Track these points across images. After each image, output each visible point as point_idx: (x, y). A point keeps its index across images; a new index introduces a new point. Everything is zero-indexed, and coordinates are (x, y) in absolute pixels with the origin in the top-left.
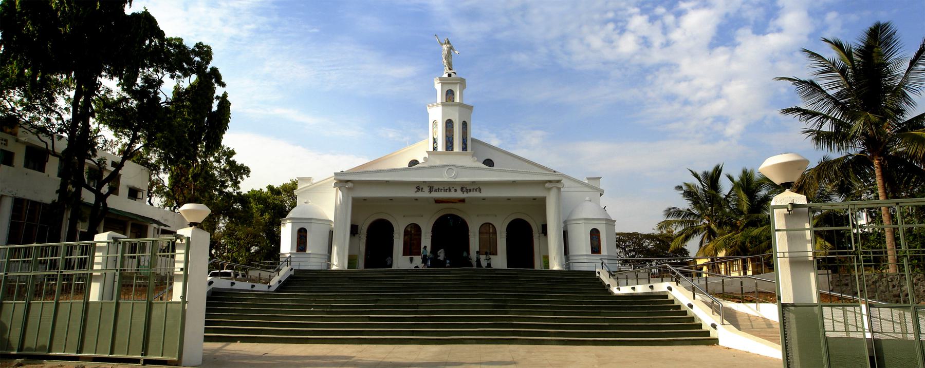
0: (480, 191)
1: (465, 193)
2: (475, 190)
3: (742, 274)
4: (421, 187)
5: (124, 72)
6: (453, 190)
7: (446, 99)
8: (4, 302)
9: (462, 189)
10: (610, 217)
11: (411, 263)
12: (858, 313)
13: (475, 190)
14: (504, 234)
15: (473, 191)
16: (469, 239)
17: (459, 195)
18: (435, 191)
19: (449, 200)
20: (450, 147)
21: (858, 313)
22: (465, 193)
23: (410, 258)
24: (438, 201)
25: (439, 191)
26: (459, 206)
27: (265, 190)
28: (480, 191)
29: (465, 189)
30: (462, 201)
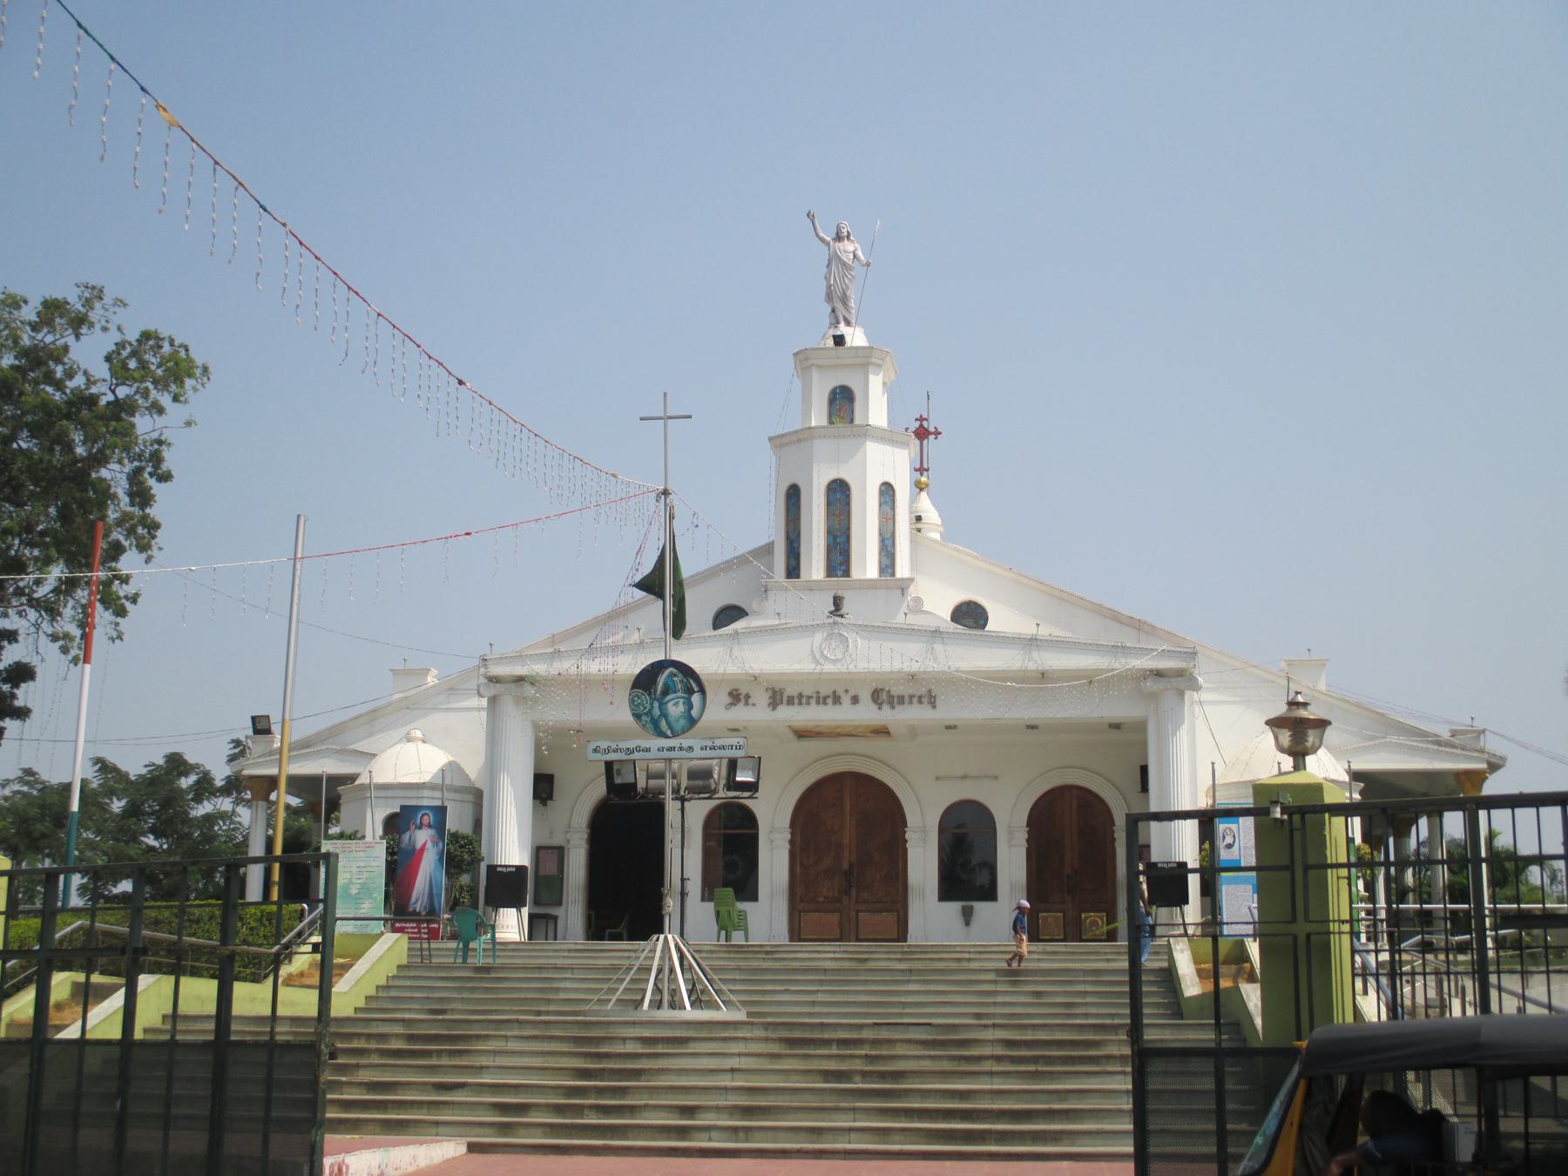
0: (933, 703)
1: (886, 707)
2: (915, 700)
3: (460, 960)
4: (743, 691)
5: (20, 896)
6: (846, 699)
7: (830, 415)
8: (174, 961)
9: (876, 696)
10: (1209, 789)
11: (967, 924)
12: (1431, 987)
13: (915, 700)
14: (1022, 836)
15: (911, 702)
16: (905, 850)
17: (866, 714)
18: (790, 701)
19: (838, 730)
20: (841, 565)
21: (1431, 987)
22: (886, 707)
23: (964, 908)
24: (802, 734)
25: (800, 703)
26: (877, 746)
27: (157, 534)
28: (933, 703)
29: (884, 696)
30: (882, 732)
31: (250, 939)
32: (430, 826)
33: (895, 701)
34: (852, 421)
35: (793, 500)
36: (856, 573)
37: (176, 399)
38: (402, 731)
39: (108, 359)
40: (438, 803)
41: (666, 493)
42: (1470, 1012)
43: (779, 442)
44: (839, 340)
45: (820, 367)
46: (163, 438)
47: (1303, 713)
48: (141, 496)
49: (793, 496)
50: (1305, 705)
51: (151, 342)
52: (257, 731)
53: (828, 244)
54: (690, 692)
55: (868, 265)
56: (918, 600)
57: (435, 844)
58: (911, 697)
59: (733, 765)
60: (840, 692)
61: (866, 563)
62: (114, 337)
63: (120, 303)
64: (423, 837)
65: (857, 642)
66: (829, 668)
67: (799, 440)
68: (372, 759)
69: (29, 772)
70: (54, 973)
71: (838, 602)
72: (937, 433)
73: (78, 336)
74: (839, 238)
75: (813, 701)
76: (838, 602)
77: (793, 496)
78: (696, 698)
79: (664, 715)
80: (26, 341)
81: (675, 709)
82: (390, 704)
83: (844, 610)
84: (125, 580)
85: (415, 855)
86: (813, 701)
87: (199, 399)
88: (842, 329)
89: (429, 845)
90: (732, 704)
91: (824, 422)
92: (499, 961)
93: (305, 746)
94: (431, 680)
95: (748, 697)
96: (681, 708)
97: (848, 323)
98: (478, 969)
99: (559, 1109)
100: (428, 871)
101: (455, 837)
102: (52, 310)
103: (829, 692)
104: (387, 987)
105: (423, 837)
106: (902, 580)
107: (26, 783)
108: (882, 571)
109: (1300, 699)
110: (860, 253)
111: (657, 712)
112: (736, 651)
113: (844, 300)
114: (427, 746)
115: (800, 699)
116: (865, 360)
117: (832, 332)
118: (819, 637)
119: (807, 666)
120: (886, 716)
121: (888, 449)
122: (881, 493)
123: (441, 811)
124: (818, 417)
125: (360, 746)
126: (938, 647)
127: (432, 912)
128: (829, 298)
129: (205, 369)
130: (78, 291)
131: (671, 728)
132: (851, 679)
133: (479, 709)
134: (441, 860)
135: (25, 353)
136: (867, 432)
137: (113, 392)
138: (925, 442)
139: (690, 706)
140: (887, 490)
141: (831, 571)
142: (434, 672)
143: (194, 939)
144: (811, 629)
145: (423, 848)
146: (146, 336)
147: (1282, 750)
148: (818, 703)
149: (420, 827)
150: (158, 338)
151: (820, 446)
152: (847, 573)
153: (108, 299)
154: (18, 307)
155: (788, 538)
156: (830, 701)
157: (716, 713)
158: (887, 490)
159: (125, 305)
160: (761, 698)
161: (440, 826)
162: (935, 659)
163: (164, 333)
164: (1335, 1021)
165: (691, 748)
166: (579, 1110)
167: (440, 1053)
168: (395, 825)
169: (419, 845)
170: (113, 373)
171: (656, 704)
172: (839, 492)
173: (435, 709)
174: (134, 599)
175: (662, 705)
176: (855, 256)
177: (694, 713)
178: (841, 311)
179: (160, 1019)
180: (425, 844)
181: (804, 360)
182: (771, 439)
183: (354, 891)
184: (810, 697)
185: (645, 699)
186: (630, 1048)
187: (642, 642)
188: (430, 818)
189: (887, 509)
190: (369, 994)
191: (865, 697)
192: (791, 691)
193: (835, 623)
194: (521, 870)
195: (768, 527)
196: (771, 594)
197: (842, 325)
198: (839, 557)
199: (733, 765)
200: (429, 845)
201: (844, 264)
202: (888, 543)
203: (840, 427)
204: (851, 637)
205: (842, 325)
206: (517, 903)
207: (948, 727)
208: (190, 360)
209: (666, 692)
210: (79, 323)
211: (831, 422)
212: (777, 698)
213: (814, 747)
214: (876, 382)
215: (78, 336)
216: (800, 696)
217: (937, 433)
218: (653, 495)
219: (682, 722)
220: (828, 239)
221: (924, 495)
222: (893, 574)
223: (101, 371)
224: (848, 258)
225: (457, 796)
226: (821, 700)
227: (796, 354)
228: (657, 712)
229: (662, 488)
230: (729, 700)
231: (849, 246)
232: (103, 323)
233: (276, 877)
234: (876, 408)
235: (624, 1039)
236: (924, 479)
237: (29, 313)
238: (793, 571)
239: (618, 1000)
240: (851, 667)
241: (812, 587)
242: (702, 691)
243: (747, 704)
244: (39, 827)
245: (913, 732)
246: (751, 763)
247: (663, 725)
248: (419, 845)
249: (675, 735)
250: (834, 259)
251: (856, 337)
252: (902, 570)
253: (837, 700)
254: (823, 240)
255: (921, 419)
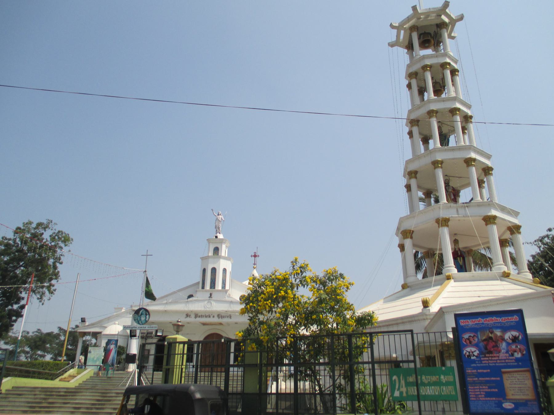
0: (230, 317)
1: (220, 318)
2: (227, 317)
4: (189, 314)
6: (212, 317)
13: (227, 317)
17: (216, 320)
18: (199, 317)
22: (220, 318)
24: (204, 324)
25: (201, 317)
28: (230, 317)
29: (220, 316)
30: (221, 324)
31: (51, 370)
32: (114, 344)
33: (223, 317)
34: (218, 255)
35: (214, 271)
36: (216, 288)
37: (65, 246)
38: (113, 322)
39: (50, 236)
40: (116, 339)
41: (145, 271)
42: (206, 383)
43: (202, 259)
44: (216, 237)
45: (212, 243)
46: (63, 254)
47: (180, 324)
48: (55, 267)
49: (204, 270)
50: (180, 322)
51: (60, 233)
52: (82, 321)
53: (216, 216)
54: (146, 315)
55: (224, 221)
56: (229, 295)
57: (115, 348)
58: (226, 316)
59: (157, 331)
60: (210, 315)
61: (219, 286)
62: (53, 231)
63: (56, 224)
64: (112, 347)
65: (213, 303)
66: (208, 309)
67: (206, 259)
68: (104, 329)
69: (39, 330)
70: (4, 378)
71: (211, 295)
72: (258, 256)
73: (45, 231)
74: (218, 215)
75: (204, 317)
76: (211, 295)
77: (204, 270)
78: (148, 316)
79: (140, 320)
80: (33, 231)
81: (143, 318)
82: (113, 316)
83: (212, 296)
84: (53, 286)
85: (110, 351)
86: (204, 317)
87: (72, 246)
88: (218, 234)
89: (114, 349)
90: (187, 317)
91: (212, 255)
92: (114, 376)
93: (92, 325)
94: (123, 311)
95: (190, 315)
96: (144, 318)
97: (219, 233)
98: (108, 378)
99: (87, 408)
100: (113, 354)
101: (120, 347)
102: (39, 225)
103: (208, 315)
104: (85, 382)
105: (112, 347)
106: (226, 290)
107: (38, 332)
108: (222, 288)
109: (179, 320)
110: (223, 218)
111: (139, 319)
112: (187, 305)
113: (219, 228)
114: (119, 325)
115: (202, 316)
116: (222, 241)
117: (215, 235)
118: (206, 302)
119: (203, 309)
120: (221, 320)
121: (225, 261)
122: (223, 270)
123: (117, 341)
124: (211, 254)
125: (104, 325)
126: (232, 305)
127: (113, 365)
128: (216, 228)
129: (72, 240)
130: (47, 221)
131: (141, 322)
132: (213, 312)
133: (130, 317)
134: (116, 352)
135: (32, 234)
136: (221, 257)
137: (51, 244)
138: (256, 258)
139: (146, 318)
140: (225, 270)
141: (211, 288)
142: (124, 308)
143: (33, 369)
144: (203, 301)
145: (112, 350)
146: (59, 232)
147: (174, 330)
148: (205, 317)
149: (112, 344)
150: (62, 232)
151: (210, 260)
152: (214, 288)
153: (53, 222)
154: (31, 224)
155: (203, 280)
156: (208, 317)
157: (152, 319)
158: (225, 270)
159: (57, 224)
160: (193, 316)
161: (116, 344)
162: (231, 308)
163: (64, 231)
164: (174, 383)
165: (145, 327)
166: (91, 408)
167: (69, 396)
168: (108, 343)
169: (111, 349)
170: (51, 240)
171: (139, 317)
172: (214, 270)
173: (124, 317)
174: (55, 290)
175: (140, 317)
176: (222, 219)
177: (147, 319)
178: (218, 231)
179: (11, 387)
180: (112, 348)
181: (209, 241)
182: (201, 258)
183: (95, 359)
184: (203, 316)
185: (137, 316)
186: (113, 395)
187: (167, 303)
188: (114, 342)
189: (224, 274)
190: (80, 383)
191: (216, 316)
192: (200, 314)
193: (209, 299)
194: (135, 355)
195: (198, 278)
196: (197, 293)
197: (218, 234)
198: (213, 284)
199: (157, 331)
200: (114, 349)
201: (219, 221)
202: (224, 281)
203: (216, 256)
204: (212, 302)
205: (218, 234)
206: (133, 362)
207: (236, 323)
208: (69, 237)
209: (141, 314)
210: (45, 229)
211: (214, 255)
212: (196, 316)
213: (207, 327)
214: (224, 246)
215: (45, 231)
216: (202, 315)
217: (258, 256)
218: (143, 272)
219: (144, 321)
220: (216, 215)
221: (255, 270)
222: (225, 289)
223: (49, 239)
224: (220, 219)
225: (124, 337)
226: (206, 317)
227: (207, 240)
228: (139, 319)
229: (144, 270)
230: (186, 316)
231: (220, 217)
232: (51, 228)
233: (486, 365)
234: (224, 251)
235: (112, 393)
236: (255, 266)
237: (34, 225)
238: (203, 287)
239: (121, 385)
240: (212, 310)
241: (207, 291)
242: (149, 315)
243: (190, 317)
244: (38, 343)
245: (228, 324)
246: (161, 331)
247: (140, 322)
248: (111, 349)
249: (142, 324)
250: (217, 219)
251: (220, 236)
252: (227, 287)
253: (210, 317)
254: (215, 215)
255: (255, 253)
